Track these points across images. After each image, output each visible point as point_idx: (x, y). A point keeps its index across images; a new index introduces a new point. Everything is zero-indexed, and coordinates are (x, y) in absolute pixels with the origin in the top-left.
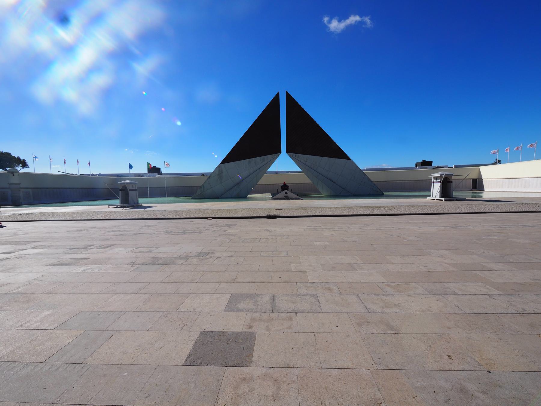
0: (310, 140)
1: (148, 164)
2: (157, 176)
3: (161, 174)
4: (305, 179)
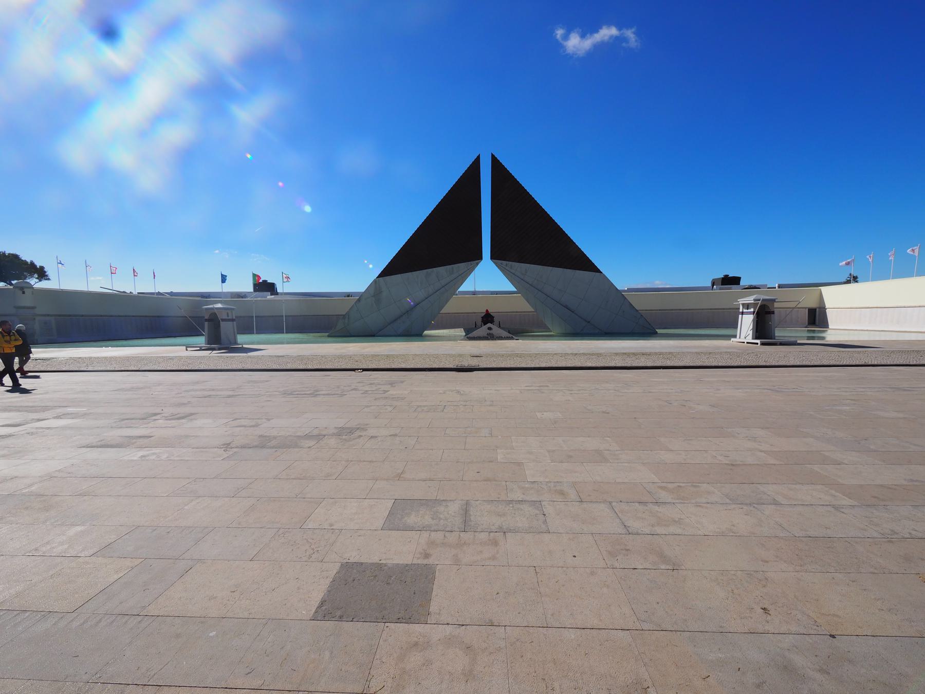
0: (532, 238)
2: (270, 297)
3: (277, 294)
4: (522, 305)
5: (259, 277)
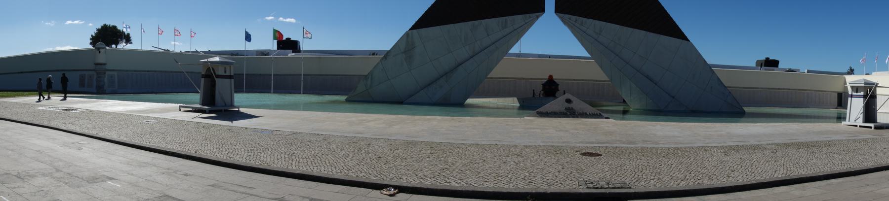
1: (275, 32)
2: (291, 54)
3: (299, 51)
5: (281, 35)
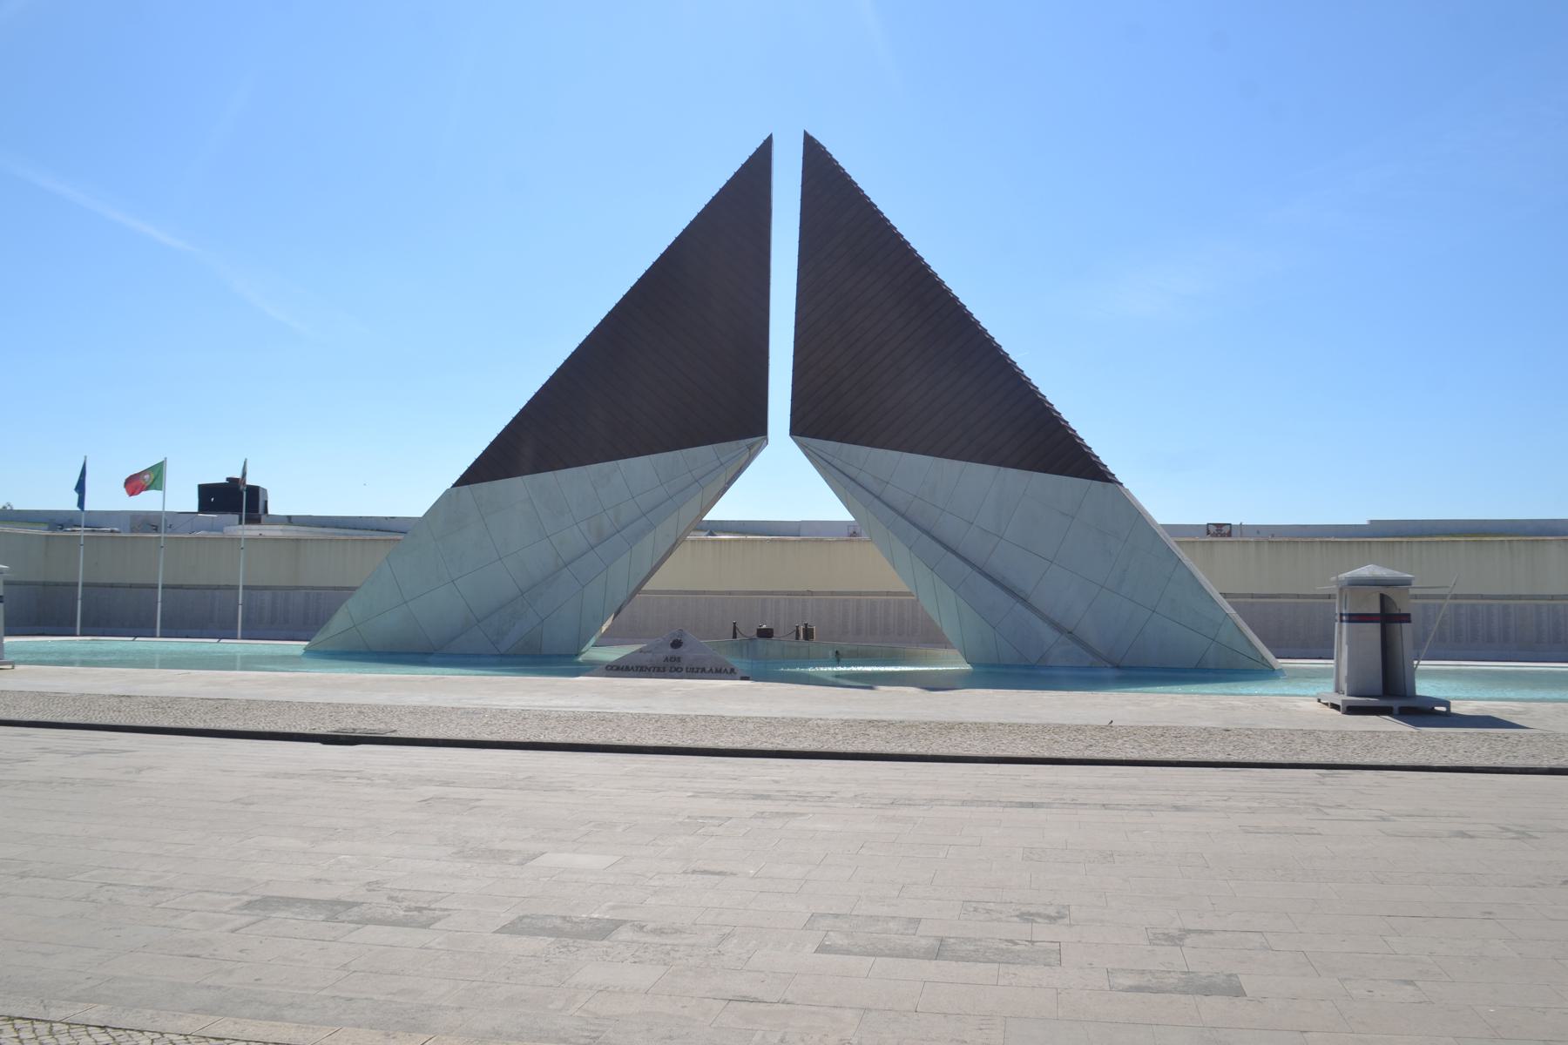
0: (912, 367)
